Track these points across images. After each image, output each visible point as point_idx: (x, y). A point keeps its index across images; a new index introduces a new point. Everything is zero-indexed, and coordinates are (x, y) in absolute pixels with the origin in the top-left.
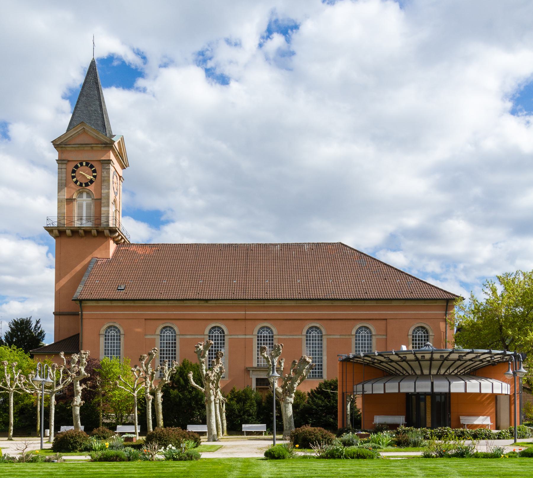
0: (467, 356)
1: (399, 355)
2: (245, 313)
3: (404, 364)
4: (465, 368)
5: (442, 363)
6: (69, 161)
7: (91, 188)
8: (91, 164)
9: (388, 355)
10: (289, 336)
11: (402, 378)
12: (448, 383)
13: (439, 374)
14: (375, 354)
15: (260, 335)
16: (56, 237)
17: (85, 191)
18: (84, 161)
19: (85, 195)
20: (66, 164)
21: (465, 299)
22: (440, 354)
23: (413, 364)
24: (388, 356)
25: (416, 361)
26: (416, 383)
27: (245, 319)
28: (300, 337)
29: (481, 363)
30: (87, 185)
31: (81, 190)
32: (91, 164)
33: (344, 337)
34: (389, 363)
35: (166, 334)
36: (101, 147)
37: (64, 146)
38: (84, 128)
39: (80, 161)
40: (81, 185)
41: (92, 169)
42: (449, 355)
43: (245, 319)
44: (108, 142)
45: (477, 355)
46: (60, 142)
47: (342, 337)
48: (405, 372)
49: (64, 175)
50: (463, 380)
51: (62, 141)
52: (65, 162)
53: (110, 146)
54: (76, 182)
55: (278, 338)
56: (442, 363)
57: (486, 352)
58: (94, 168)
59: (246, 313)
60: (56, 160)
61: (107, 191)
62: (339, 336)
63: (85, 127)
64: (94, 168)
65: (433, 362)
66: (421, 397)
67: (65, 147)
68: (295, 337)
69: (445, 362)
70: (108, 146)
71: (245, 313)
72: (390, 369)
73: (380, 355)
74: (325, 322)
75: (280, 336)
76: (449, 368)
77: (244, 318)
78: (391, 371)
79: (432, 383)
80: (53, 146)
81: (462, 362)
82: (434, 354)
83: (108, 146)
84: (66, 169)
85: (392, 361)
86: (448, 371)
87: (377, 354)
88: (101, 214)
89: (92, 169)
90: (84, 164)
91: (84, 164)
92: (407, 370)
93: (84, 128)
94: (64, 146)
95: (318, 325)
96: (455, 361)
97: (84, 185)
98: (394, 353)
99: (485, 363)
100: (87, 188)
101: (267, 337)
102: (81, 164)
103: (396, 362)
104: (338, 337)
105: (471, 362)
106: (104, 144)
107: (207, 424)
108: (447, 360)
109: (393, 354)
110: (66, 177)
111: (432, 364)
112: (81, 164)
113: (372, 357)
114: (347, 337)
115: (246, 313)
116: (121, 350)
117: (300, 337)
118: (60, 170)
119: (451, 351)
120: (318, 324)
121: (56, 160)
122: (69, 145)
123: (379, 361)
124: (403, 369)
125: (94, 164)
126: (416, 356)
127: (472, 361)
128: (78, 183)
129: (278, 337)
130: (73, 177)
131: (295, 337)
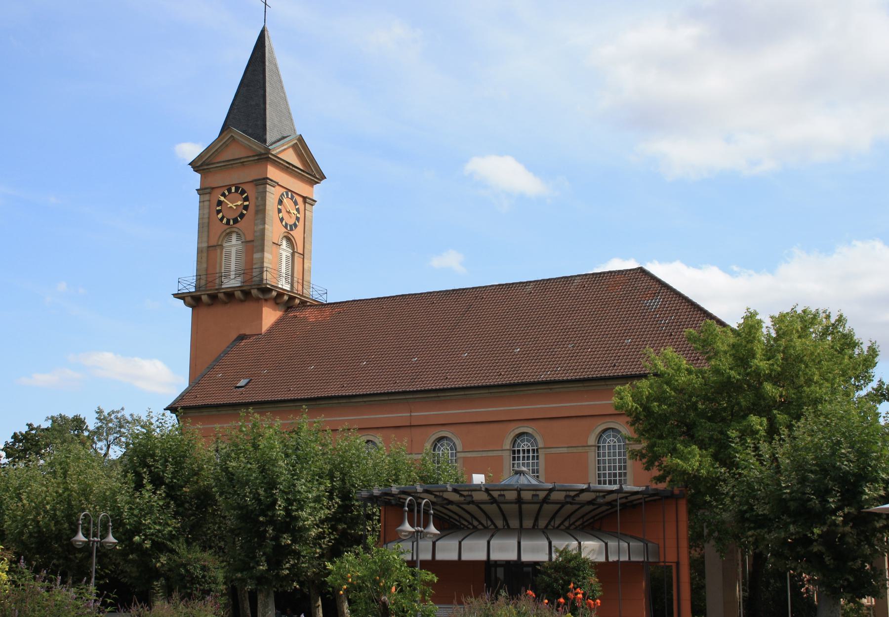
0: (580, 496)
1: (461, 492)
2: (409, 414)
3: (471, 508)
4: (583, 517)
5: (560, 509)
6: (213, 188)
7: (242, 224)
8: (242, 189)
9: (440, 492)
10: (481, 453)
11: (468, 533)
12: (546, 543)
13: (536, 527)
14: (447, 488)
15: (516, 449)
16: (193, 307)
17: (234, 232)
18: (233, 185)
19: (234, 237)
20: (210, 193)
21: (27, 425)
22: (532, 493)
23: (489, 508)
24: (441, 494)
25: (492, 503)
26: (491, 542)
27: (411, 426)
28: (499, 453)
29: (610, 509)
30: (236, 221)
31: (228, 231)
32: (242, 189)
33: (574, 450)
34: (465, 506)
35: (608, 443)
36: (254, 160)
37: (206, 167)
38: (232, 136)
39: (226, 186)
40: (228, 222)
41: (244, 196)
42: (548, 495)
43: (411, 426)
44: (263, 151)
45: (598, 494)
46: (202, 162)
47: (571, 450)
48: (475, 523)
49: (206, 211)
50: (577, 540)
51: (204, 160)
52: (208, 191)
53: (265, 156)
54: (222, 219)
55: (464, 458)
56: (560, 509)
57: (584, 488)
58: (246, 194)
59: (412, 414)
60: (197, 190)
61: (261, 227)
62: (566, 449)
63: (233, 135)
64: (246, 194)
65: (524, 506)
66: (525, 569)
67: (207, 169)
68: (490, 454)
69: (545, 506)
70: (262, 157)
71: (409, 414)
72: (450, 517)
73: (455, 490)
74: (542, 423)
75: (467, 454)
76: (553, 518)
77: (409, 424)
78: (451, 520)
79: (519, 543)
80: (192, 169)
81: (576, 507)
82: (522, 492)
83: (262, 157)
84: (209, 201)
85: (450, 502)
86: (552, 523)
87: (450, 489)
88: (252, 264)
89: (244, 196)
90: (233, 189)
91: (233, 189)
92: (480, 519)
93: (232, 136)
94: (206, 167)
95: (529, 430)
96: (563, 504)
97: (231, 222)
98: (450, 489)
99: (604, 508)
100: (237, 225)
101: (528, 451)
102: (229, 191)
103: (458, 504)
104: (565, 450)
105: (591, 507)
106: (257, 155)
107: (247, 595)
108: (548, 503)
109: (446, 491)
110: (209, 213)
111: (505, 512)
112: (229, 191)
113: (438, 494)
114: (580, 450)
115: (412, 414)
116: (540, 464)
117: (499, 453)
118: (202, 204)
119: (551, 487)
120: (529, 429)
121: (197, 190)
122: (212, 164)
123: (445, 502)
124: (473, 516)
125: (245, 187)
126: (490, 495)
127: (594, 504)
128: (225, 221)
129: (463, 455)
130: (219, 212)
131: (490, 454)
